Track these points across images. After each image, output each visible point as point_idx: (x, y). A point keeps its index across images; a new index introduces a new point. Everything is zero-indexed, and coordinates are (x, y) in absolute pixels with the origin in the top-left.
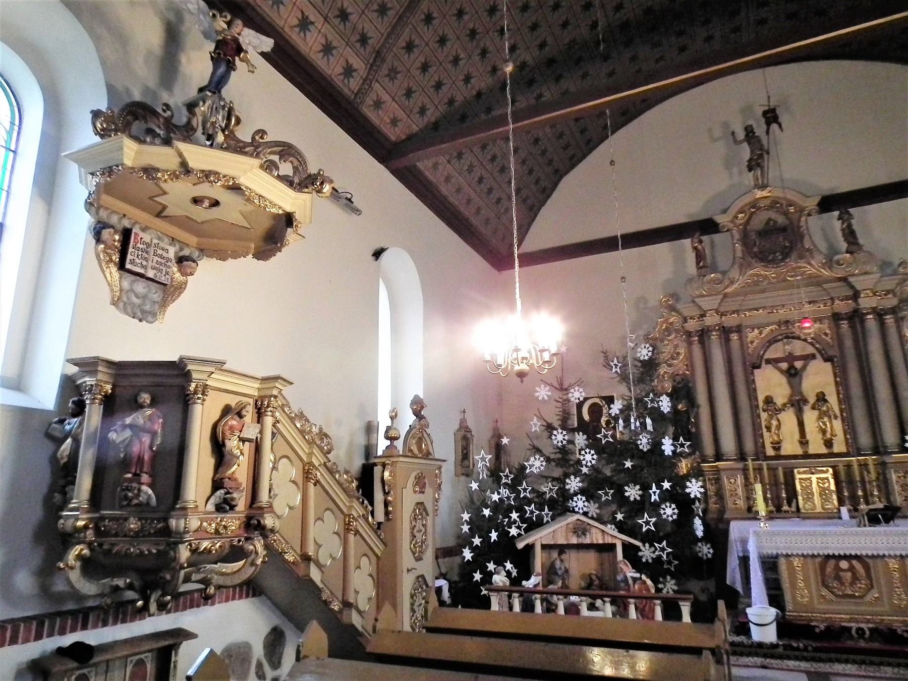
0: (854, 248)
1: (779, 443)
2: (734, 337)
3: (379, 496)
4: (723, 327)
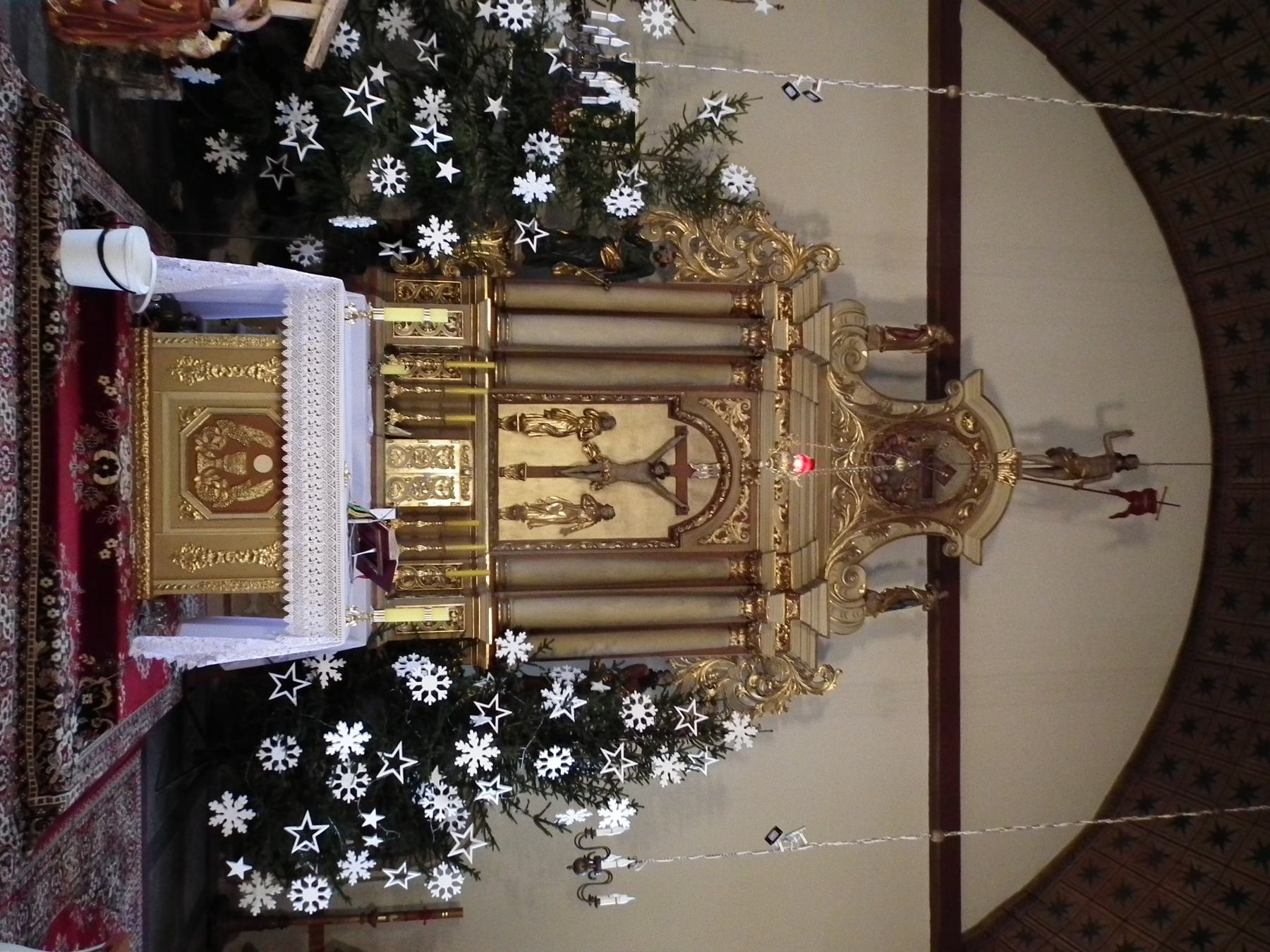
1: (522, 429)
2: (739, 377)
4: (761, 358)
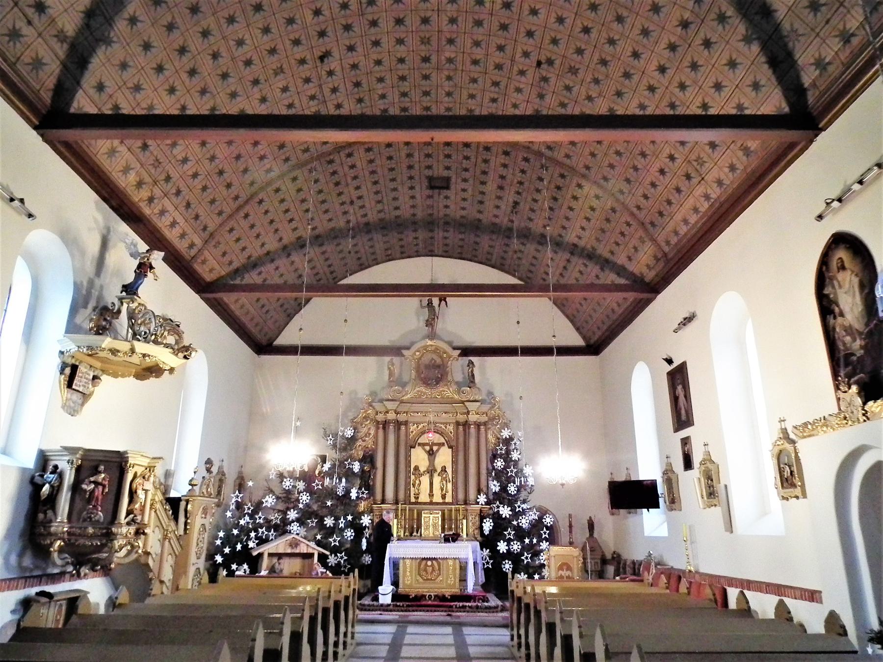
0: (472, 385)
2: (403, 428)
3: (182, 519)
